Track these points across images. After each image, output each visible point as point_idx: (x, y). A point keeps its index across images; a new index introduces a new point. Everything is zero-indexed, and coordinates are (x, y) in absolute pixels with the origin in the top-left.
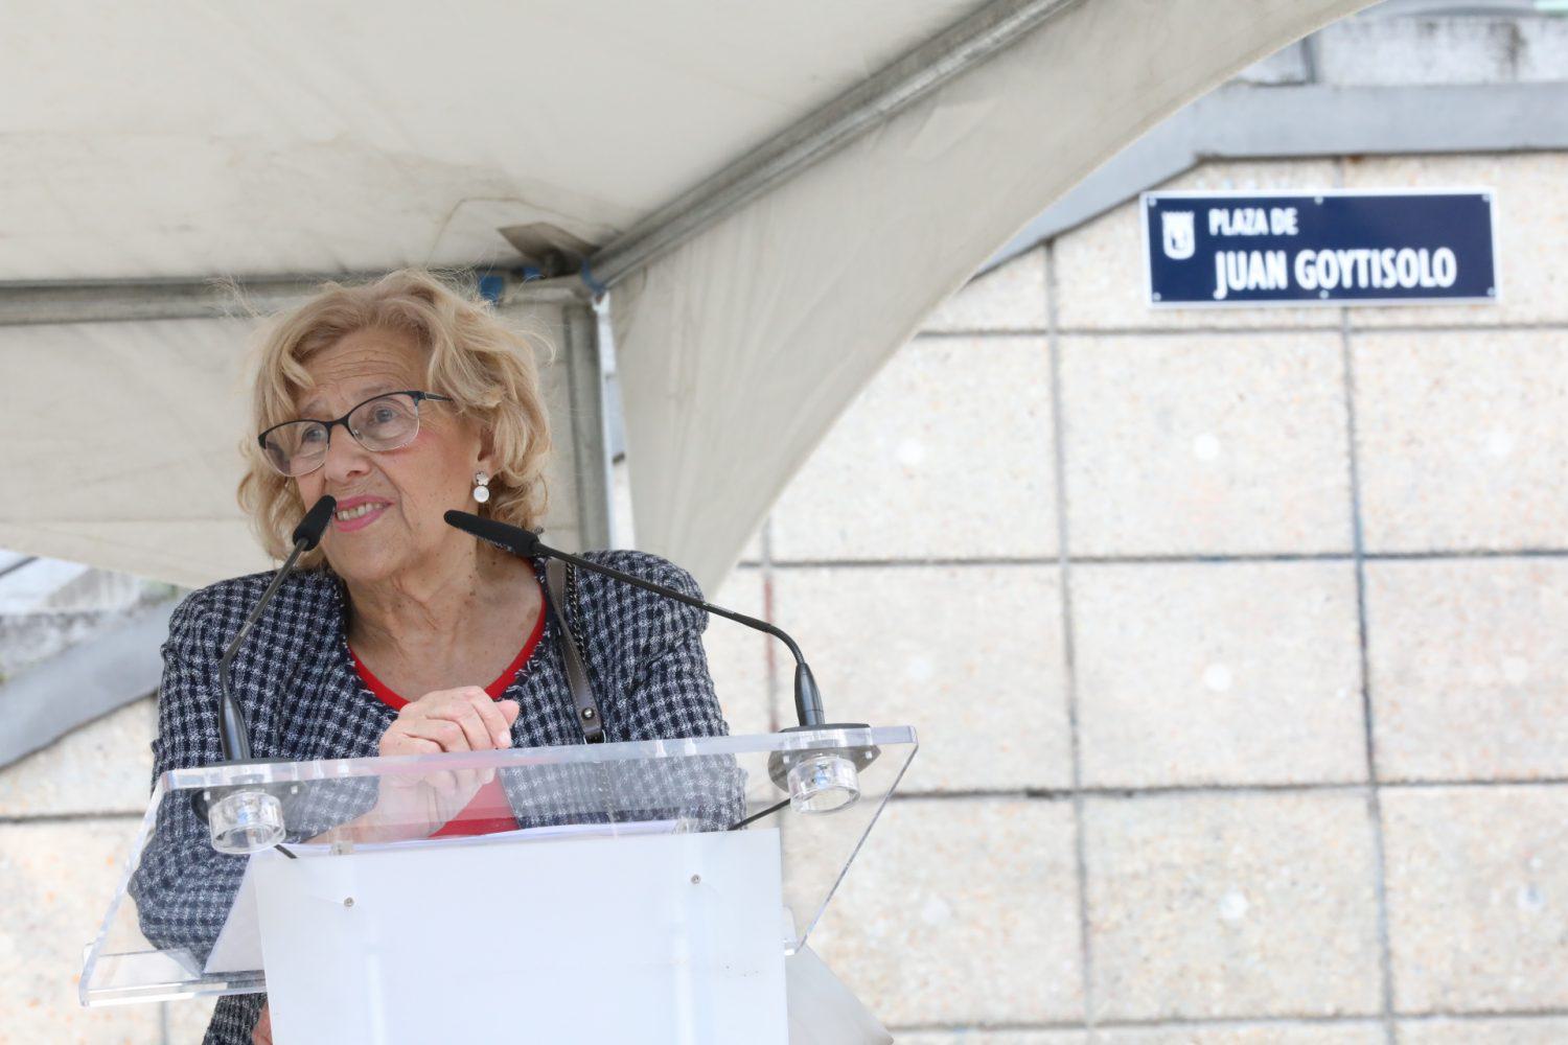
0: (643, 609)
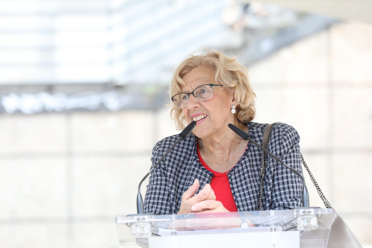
0: (277, 143)
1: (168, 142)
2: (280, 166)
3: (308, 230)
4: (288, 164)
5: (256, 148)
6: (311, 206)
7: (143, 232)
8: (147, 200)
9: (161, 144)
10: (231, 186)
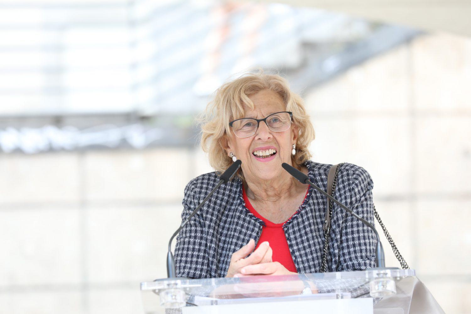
0: (347, 189)
1: (206, 181)
2: (350, 217)
3: (385, 297)
4: (360, 215)
5: (319, 195)
6: (387, 266)
7: (174, 301)
8: (177, 257)
9: (197, 183)
10: (289, 242)
